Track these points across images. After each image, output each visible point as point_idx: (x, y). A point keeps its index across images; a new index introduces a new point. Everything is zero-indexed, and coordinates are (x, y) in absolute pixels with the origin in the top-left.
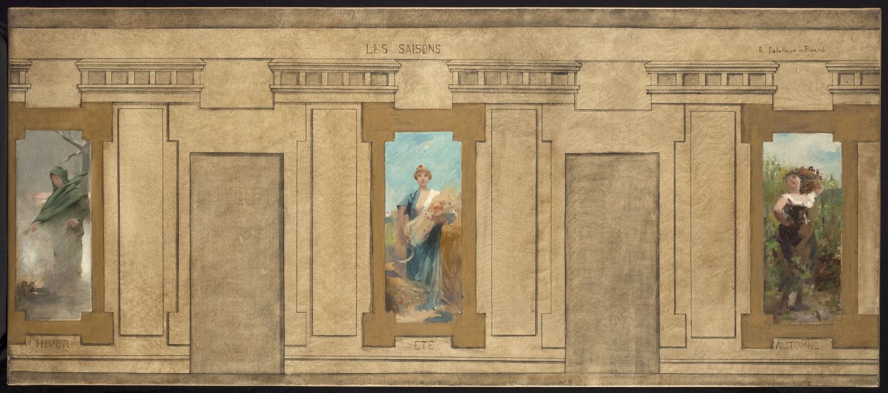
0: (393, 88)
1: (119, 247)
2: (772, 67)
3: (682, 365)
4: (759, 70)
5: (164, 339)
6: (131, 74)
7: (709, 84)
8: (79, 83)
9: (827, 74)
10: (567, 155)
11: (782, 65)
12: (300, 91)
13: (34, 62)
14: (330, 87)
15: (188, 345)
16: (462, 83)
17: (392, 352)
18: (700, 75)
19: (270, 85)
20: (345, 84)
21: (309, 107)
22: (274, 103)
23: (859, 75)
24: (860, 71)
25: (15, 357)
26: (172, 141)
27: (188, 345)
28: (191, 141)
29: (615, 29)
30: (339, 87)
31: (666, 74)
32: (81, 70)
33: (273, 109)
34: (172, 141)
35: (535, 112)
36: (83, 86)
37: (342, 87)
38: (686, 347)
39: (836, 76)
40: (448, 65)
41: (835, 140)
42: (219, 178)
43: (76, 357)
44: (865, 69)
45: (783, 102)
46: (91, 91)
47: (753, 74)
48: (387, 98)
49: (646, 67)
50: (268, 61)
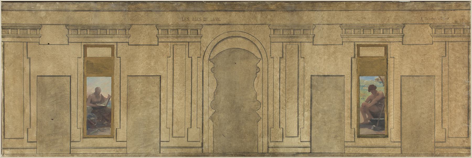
0: (402, 35)
2: (39, 27)
4: (22, 27)
6: (89, 31)
8: (157, 34)
11: (406, 25)
15: (309, 141)
16: (394, 33)
18: (371, 30)
20: (9, 33)
22: (158, 42)
25: (269, 147)
26: (119, 57)
27: (309, 141)
30: (166, 35)
32: (157, 28)
33: (69, 45)
34: (119, 57)
35: (297, 45)
38: (283, 141)
47: (31, 29)
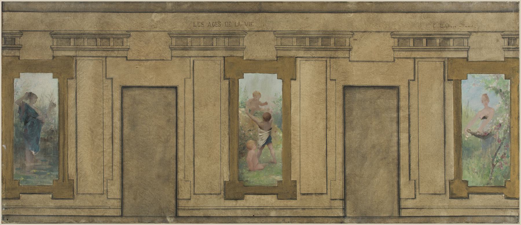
1: (194, 143)
3: (483, 210)
5: (105, 196)
7: (428, 45)
9: (503, 40)
10: (124, 88)
12: (312, 49)
13: (355, 33)
14: (323, 47)
17: (240, 203)
19: (51, 46)
21: (192, 59)
23: (412, 40)
24: (508, 37)
28: (320, 78)
29: (171, 13)
31: (404, 39)
36: (53, 47)
37: (212, 47)
39: (396, 40)
40: (275, 34)
41: (19, 77)
42: (164, 100)
43: (489, 207)
44: (513, 36)
45: (473, 56)
46: (58, 49)
48: (464, 55)
49: (502, 35)
50: (50, 32)
